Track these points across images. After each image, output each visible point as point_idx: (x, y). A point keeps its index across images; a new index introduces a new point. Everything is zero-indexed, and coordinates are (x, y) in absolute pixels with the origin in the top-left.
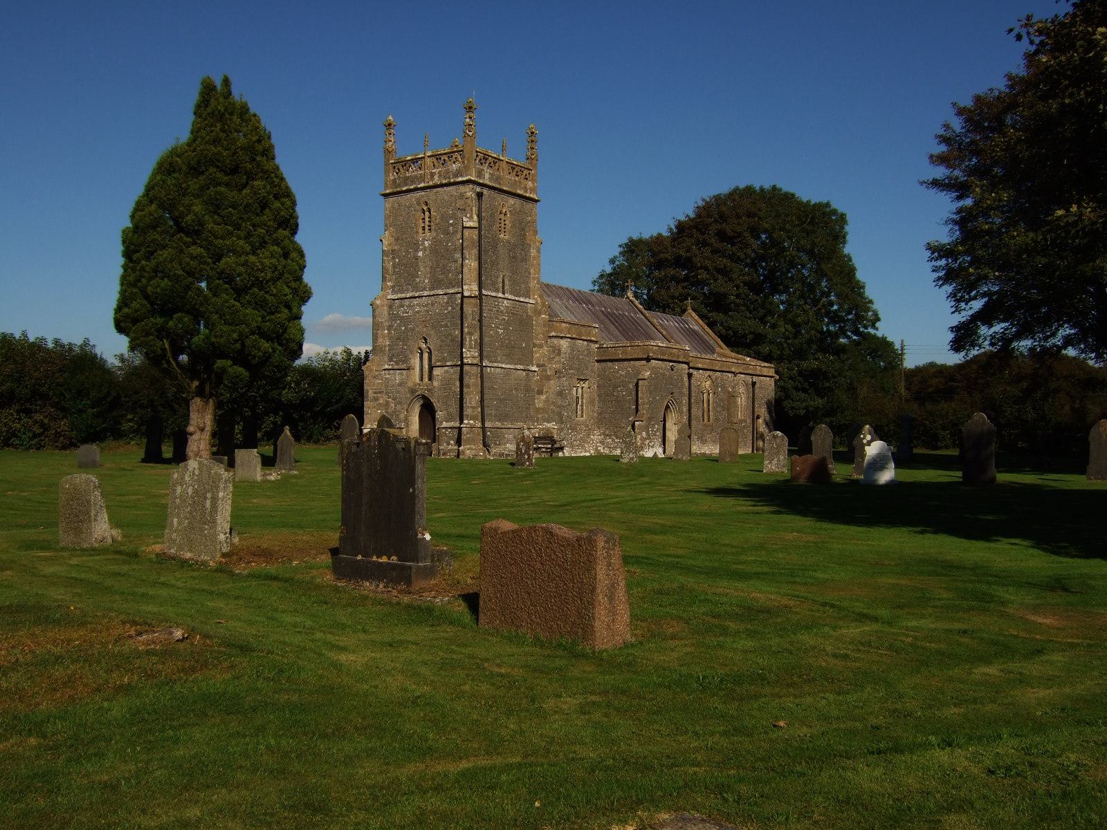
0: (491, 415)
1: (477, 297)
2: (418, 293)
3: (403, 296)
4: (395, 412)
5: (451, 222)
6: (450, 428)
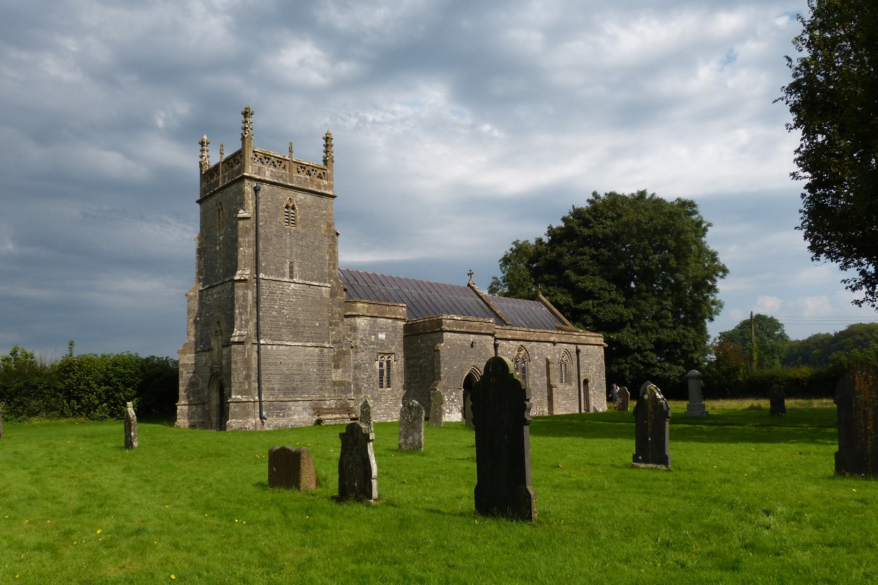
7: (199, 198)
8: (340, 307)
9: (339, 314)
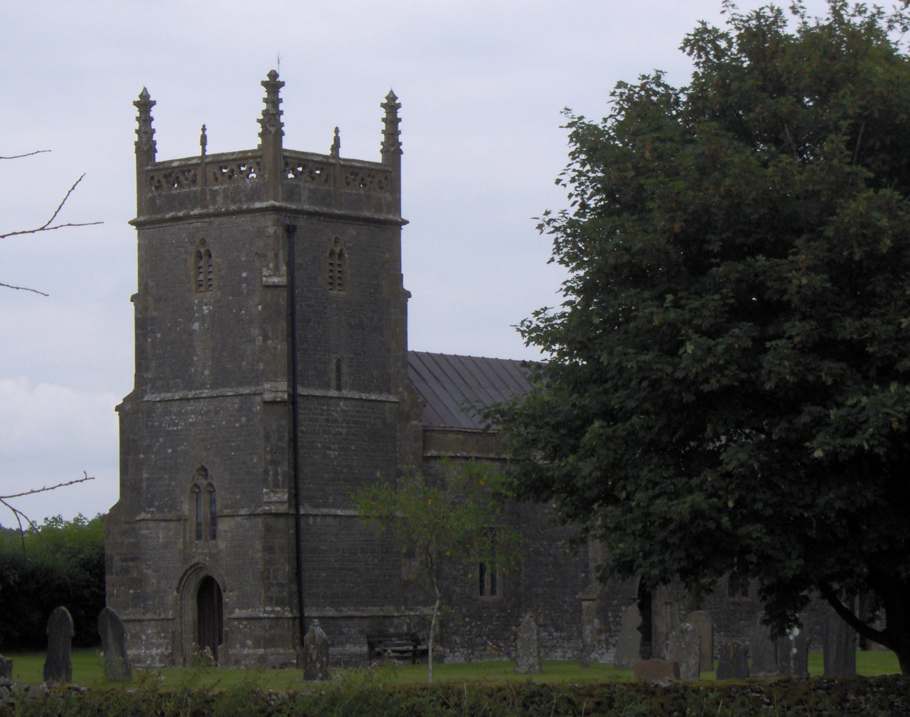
1: (285, 402)
2: (193, 392)
3: (168, 396)
5: (244, 275)
6: (246, 619)
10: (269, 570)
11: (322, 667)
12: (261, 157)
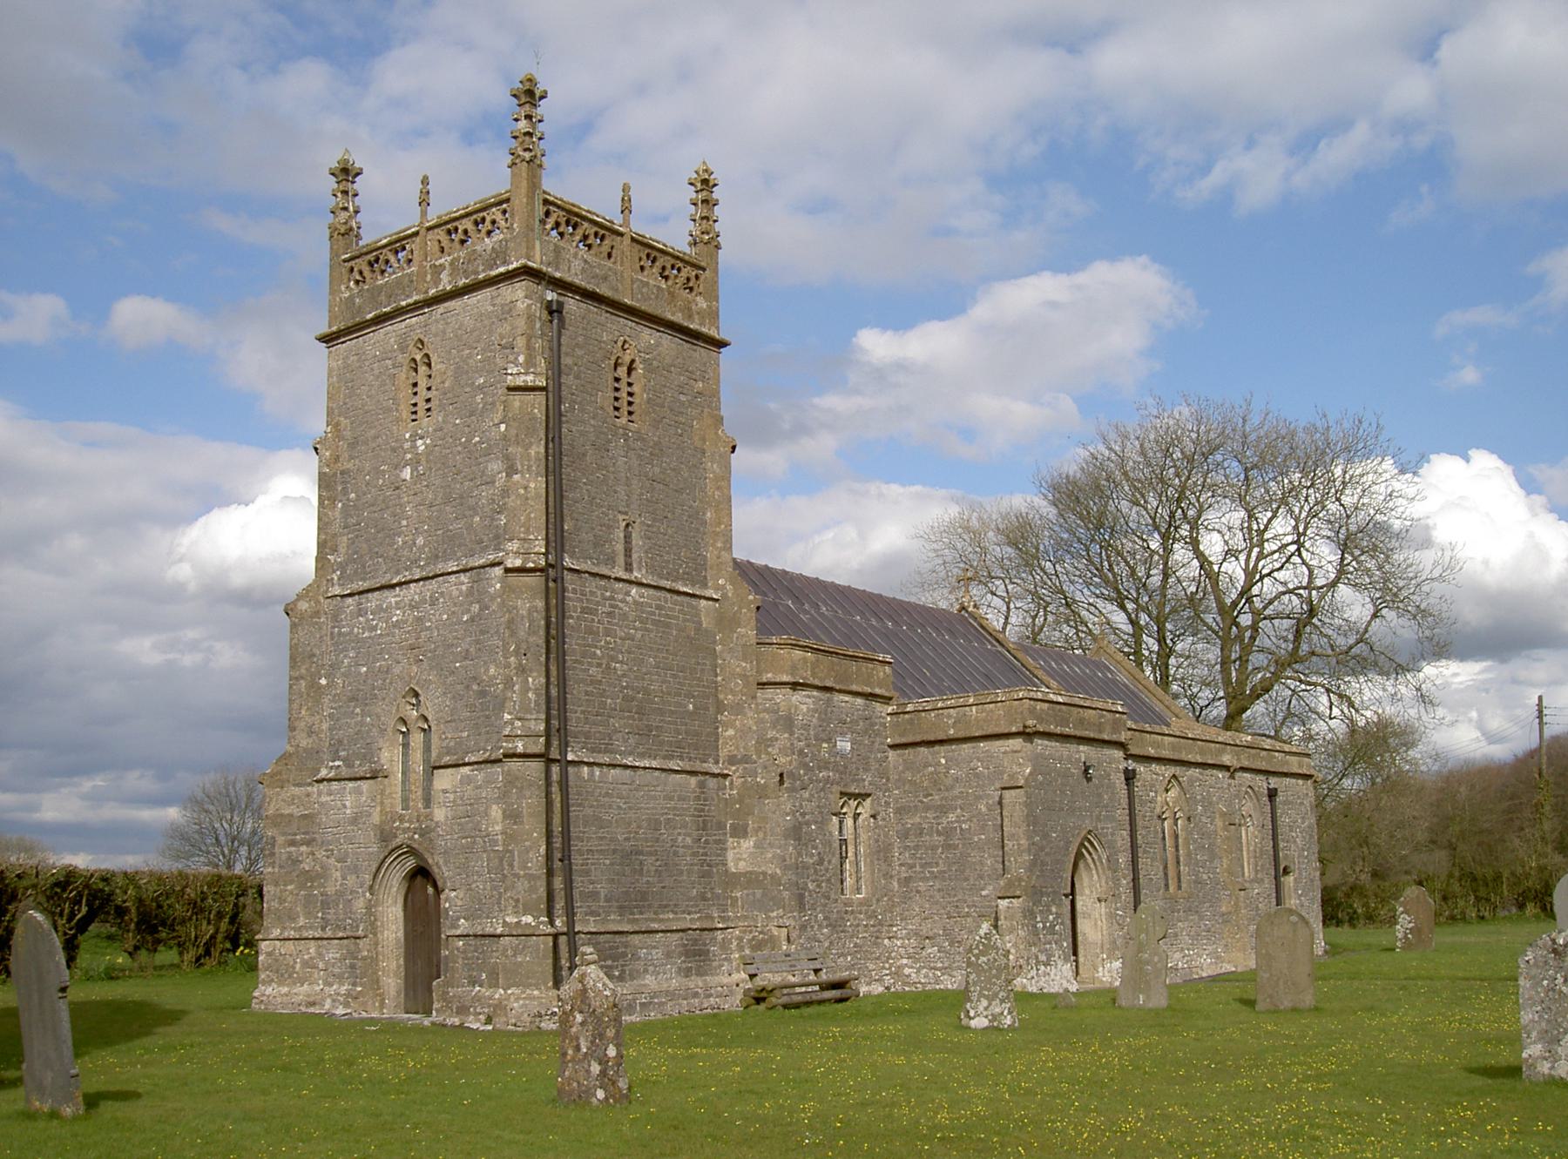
0: (594, 895)
4: (340, 894)
7: (325, 329)
8: (745, 659)
9: (744, 677)
10: (511, 852)
11: (603, 1073)
12: (507, 200)
